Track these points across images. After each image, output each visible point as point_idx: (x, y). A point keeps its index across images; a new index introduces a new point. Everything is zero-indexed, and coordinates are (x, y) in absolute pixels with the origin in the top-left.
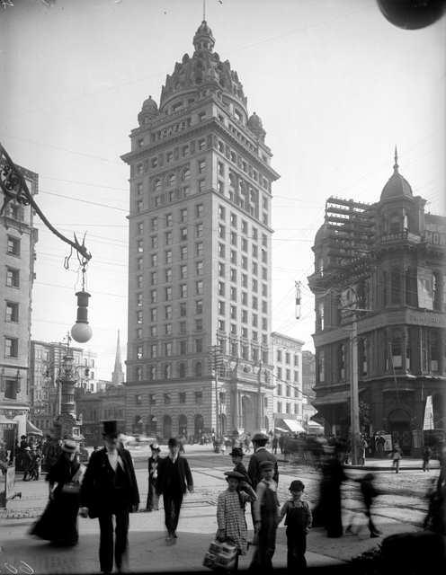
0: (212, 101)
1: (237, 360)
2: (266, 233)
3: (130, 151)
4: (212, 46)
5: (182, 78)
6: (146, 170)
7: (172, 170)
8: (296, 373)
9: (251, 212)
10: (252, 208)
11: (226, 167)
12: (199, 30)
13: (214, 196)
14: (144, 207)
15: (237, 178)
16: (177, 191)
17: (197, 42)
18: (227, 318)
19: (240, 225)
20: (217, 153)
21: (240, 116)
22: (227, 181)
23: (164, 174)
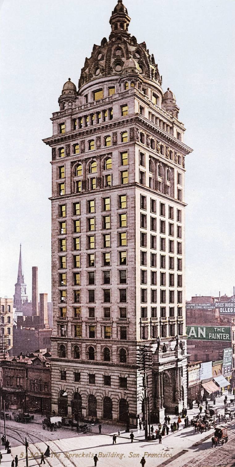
3: (51, 135)
12: (115, 9)
14: (66, 190)
15: (156, 163)
16: (99, 180)
21: (157, 97)
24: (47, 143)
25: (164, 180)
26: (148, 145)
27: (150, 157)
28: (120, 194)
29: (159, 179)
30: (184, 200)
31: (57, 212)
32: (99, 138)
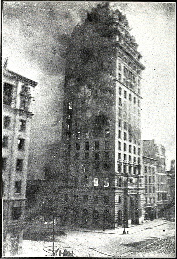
8: (120, 148)
19: (123, 93)
20: (118, 59)
22: (122, 73)
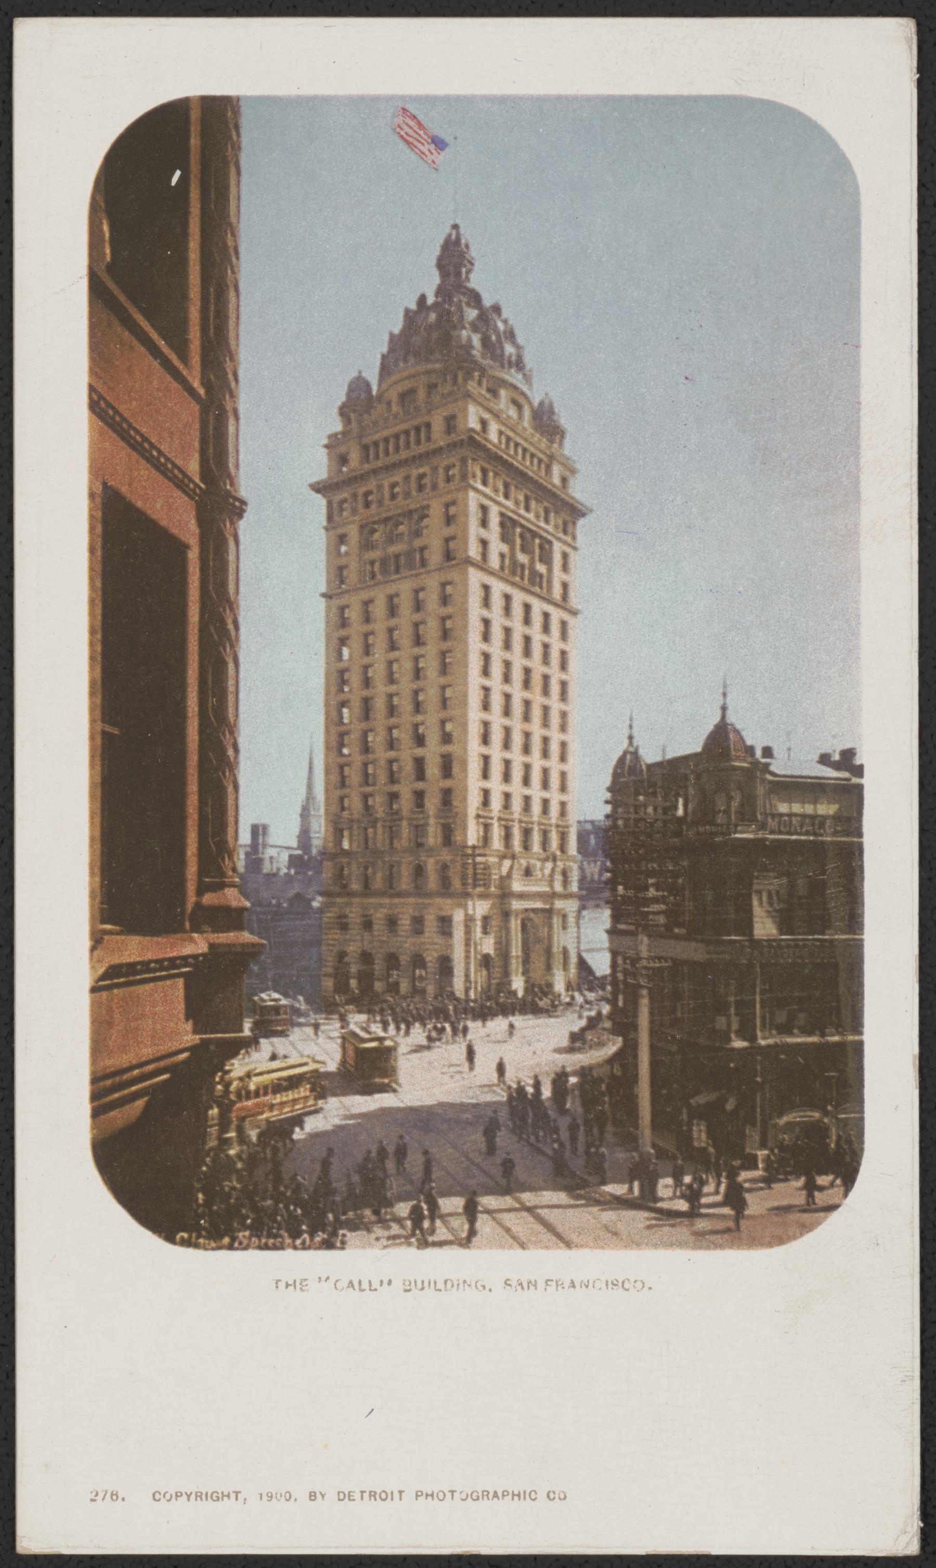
0: (468, 395)
1: (513, 857)
2: (566, 617)
4: (469, 272)
5: (417, 341)
6: (354, 511)
7: (399, 515)
9: (536, 582)
10: (541, 576)
11: (494, 510)
13: (472, 571)
17: (441, 265)
18: (496, 785)
20: (476, 490)
21: (519, 407)
22: (493, 534)
23: (386, 520)
24: (318, 491)
25: (532, 561)
26: (556, 527)
27: (502, 514)
28: (443, 579)
29: (522, 558)
30: (575, 601)
31: (335, 618)
32: (407, 478)
